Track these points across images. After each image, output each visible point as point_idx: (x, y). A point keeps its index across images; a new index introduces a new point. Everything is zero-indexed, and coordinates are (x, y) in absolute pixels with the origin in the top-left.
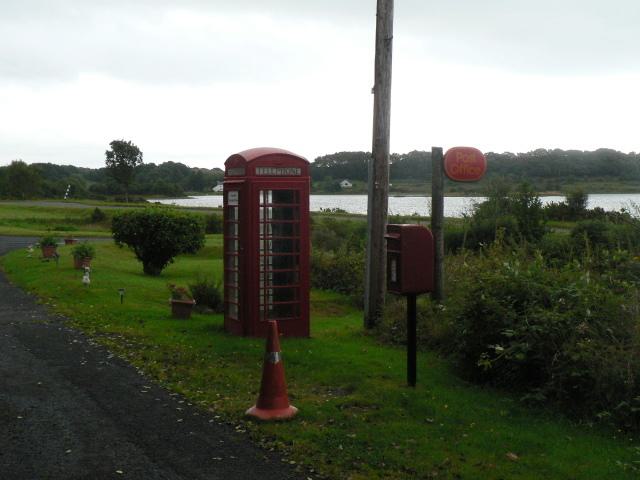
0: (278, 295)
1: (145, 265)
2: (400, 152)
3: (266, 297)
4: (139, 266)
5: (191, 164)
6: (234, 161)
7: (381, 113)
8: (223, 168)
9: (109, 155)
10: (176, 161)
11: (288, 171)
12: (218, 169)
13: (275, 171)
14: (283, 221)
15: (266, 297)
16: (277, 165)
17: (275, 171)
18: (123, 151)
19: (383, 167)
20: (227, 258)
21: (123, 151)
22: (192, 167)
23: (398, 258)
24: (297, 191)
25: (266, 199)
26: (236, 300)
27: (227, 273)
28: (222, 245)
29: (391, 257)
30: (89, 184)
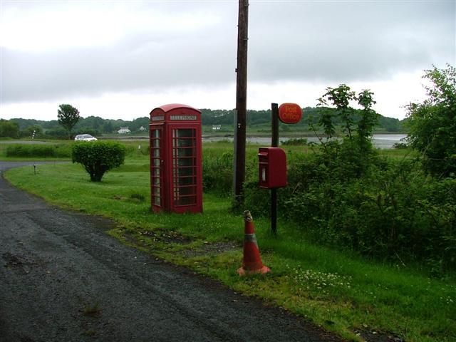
0: (182, 191)
1: (92, 176)
2: (258, 109)
3: (176, 194)
4: (87, 176)
5: (104, 117)
6: (156, 112)
7: (241, 83)
8: (149, 116)
9: (60, 112)
10: (13, 118)
11: (189, 118)
12: (54, 119)
13: (182, 118)
14: (324, 140)
15: (176, 194)
16: (183, 114)
17: (182, 118)
18: (274, 105)
19: (278, 110)
20: (153, 170)
21: (274, 105)
22: (105, 119)
23: (267, 167)
24: (195, 129)
25: (175, 134)
26: (159, 195)
27: (153, 180)
28: (149, 163)
29: (261, 167)
30: (44, 131)
